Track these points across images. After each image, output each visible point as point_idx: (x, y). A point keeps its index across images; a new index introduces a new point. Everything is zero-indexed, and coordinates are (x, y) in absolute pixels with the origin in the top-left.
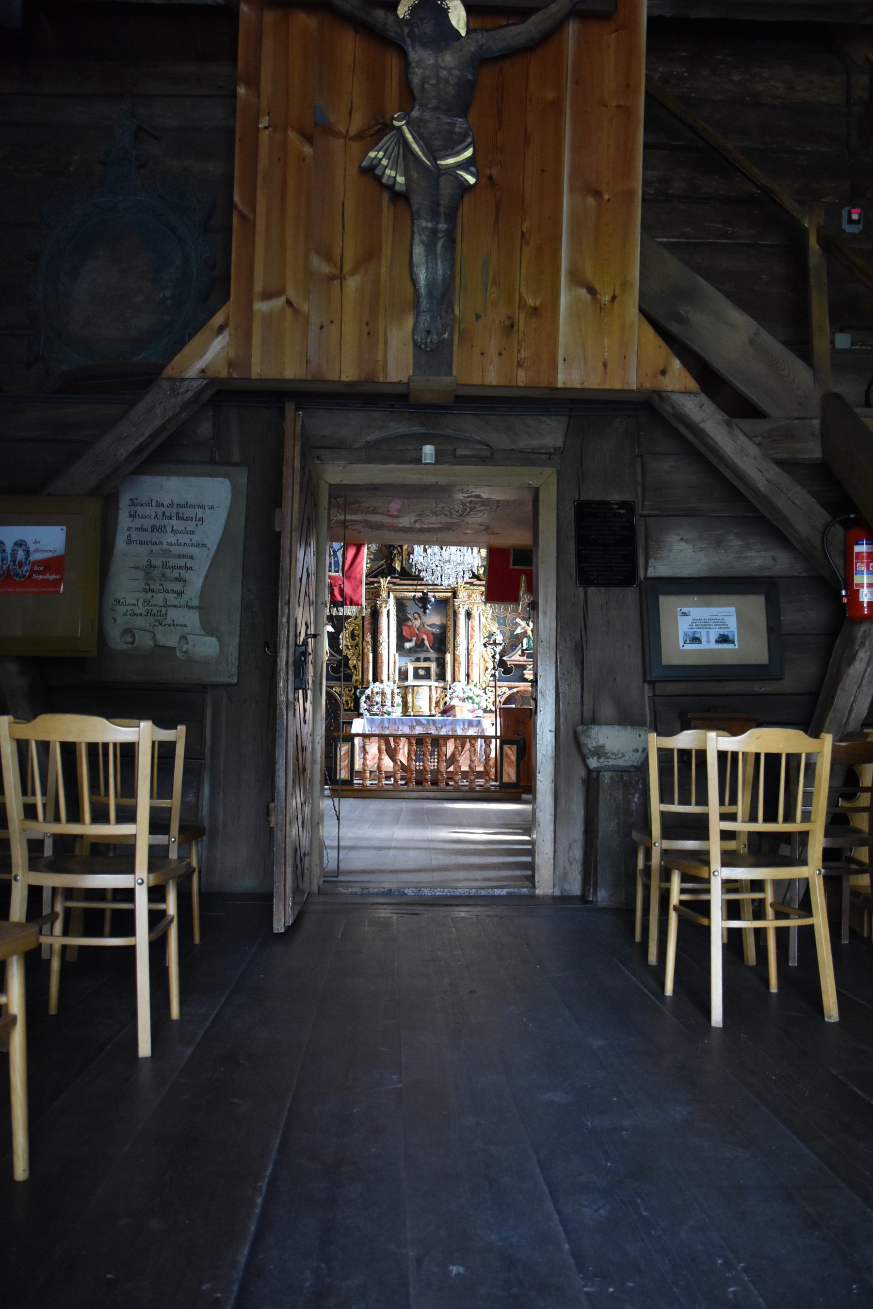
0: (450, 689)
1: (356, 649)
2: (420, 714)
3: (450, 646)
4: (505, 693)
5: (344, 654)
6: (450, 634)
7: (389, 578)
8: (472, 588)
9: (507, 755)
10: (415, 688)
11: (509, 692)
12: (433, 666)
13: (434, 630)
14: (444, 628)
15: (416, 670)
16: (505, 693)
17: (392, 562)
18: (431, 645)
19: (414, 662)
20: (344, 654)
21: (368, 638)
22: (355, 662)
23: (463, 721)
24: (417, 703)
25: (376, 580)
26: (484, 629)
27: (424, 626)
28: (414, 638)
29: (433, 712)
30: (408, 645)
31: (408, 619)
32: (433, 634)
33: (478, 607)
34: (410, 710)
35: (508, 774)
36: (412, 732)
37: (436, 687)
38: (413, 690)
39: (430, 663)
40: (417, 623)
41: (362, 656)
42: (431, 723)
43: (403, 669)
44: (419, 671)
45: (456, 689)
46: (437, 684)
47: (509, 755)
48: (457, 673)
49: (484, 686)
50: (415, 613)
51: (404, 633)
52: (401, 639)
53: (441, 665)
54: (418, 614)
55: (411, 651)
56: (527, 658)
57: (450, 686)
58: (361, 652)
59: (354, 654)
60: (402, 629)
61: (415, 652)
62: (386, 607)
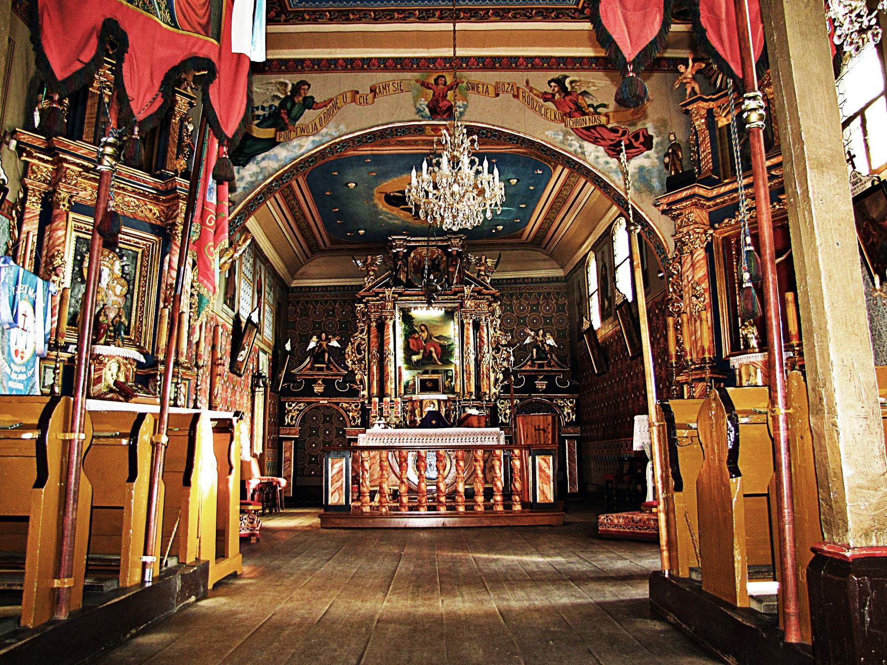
7: (394, 288)
9: (541, 470)
15: (423, 382)
17: (396, 274)
18: (439, 357)
25: (380, 290)
28: (422, 351)
30: (415, 358)
35: (543, 492)
40: (425, 335)
47: (543, 468)
51: (411, 346)
52: (409, 352)
61: (423, 364)
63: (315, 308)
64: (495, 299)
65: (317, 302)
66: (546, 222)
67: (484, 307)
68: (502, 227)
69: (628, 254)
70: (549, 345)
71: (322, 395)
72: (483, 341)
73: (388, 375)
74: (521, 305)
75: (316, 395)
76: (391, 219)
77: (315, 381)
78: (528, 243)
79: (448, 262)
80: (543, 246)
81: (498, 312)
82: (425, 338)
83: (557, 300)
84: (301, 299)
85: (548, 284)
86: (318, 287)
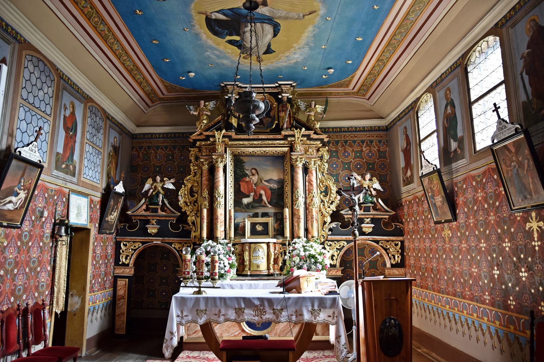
0: (289, 244)
1: (195, 205)
2: (258, 273)
3: (288, 201)
4: (343, 247)
5: (183, 210)
6: (288, 189)
7: (224, 131)
8: (308, 142)
10: (252, 245)
11: (347, 246)
12: (270, 220)
13: (272, 185)
14: (281, 183)
15: (253, 225)
16: (343, 247)
17: (228, 119)
18: (269, 200)
19: (252, 217)
20: (183, 210)
21: (206, 194)
22: (193, 218)
23: (312, 300)
24: (255, 262)
26: (321, 184)
27: (261, 181)
28: (252, 194)
29: (272, 271)
30: (246, 201)
31: (246, 175)
32: (271, 189)
33: (315, 161)
34: (247, 269)
36: (239, 317)
37: (274, 243)
38: (250, 248)
39: (267, 219)
40: (255, 179)
41: (199, 213)
42: (266, 304)
43: (241, 225)
44: (257, 227)
45: (296, 246)
46: (275, 240)
48: (296, 228)
49: (322, 240)
50: (252, 169)
52: (239, 195)
53: (280, 219)
54: (255, 169)
55: (248, 205)
56: (364, 212)
57: (289, 242)
58: (199, 208)
59: (192, 210)
60: (239, 185)
61: (253, 207)
62: (222, 161)
63: (156, 153)
64: (324, 145)
65: (158, 147)
66: (378, 65)
67: (312, 151)
68: (332, 70)
69: (419, 119)
70: (375, 189)
71: (156, 235)
72: (312, 185)
73: (217, 219)
74: (345, 151)
75: (150, 235)
76: (218, 57)
77: (148, 222)
78: (353, 93)
79: (278, 108)
80: (367, 97)
81: (326, 157)
82: (255, 182)
83: (379, 147)
84: (143, 145)
85: (370, 133)
86: (159, 134)
